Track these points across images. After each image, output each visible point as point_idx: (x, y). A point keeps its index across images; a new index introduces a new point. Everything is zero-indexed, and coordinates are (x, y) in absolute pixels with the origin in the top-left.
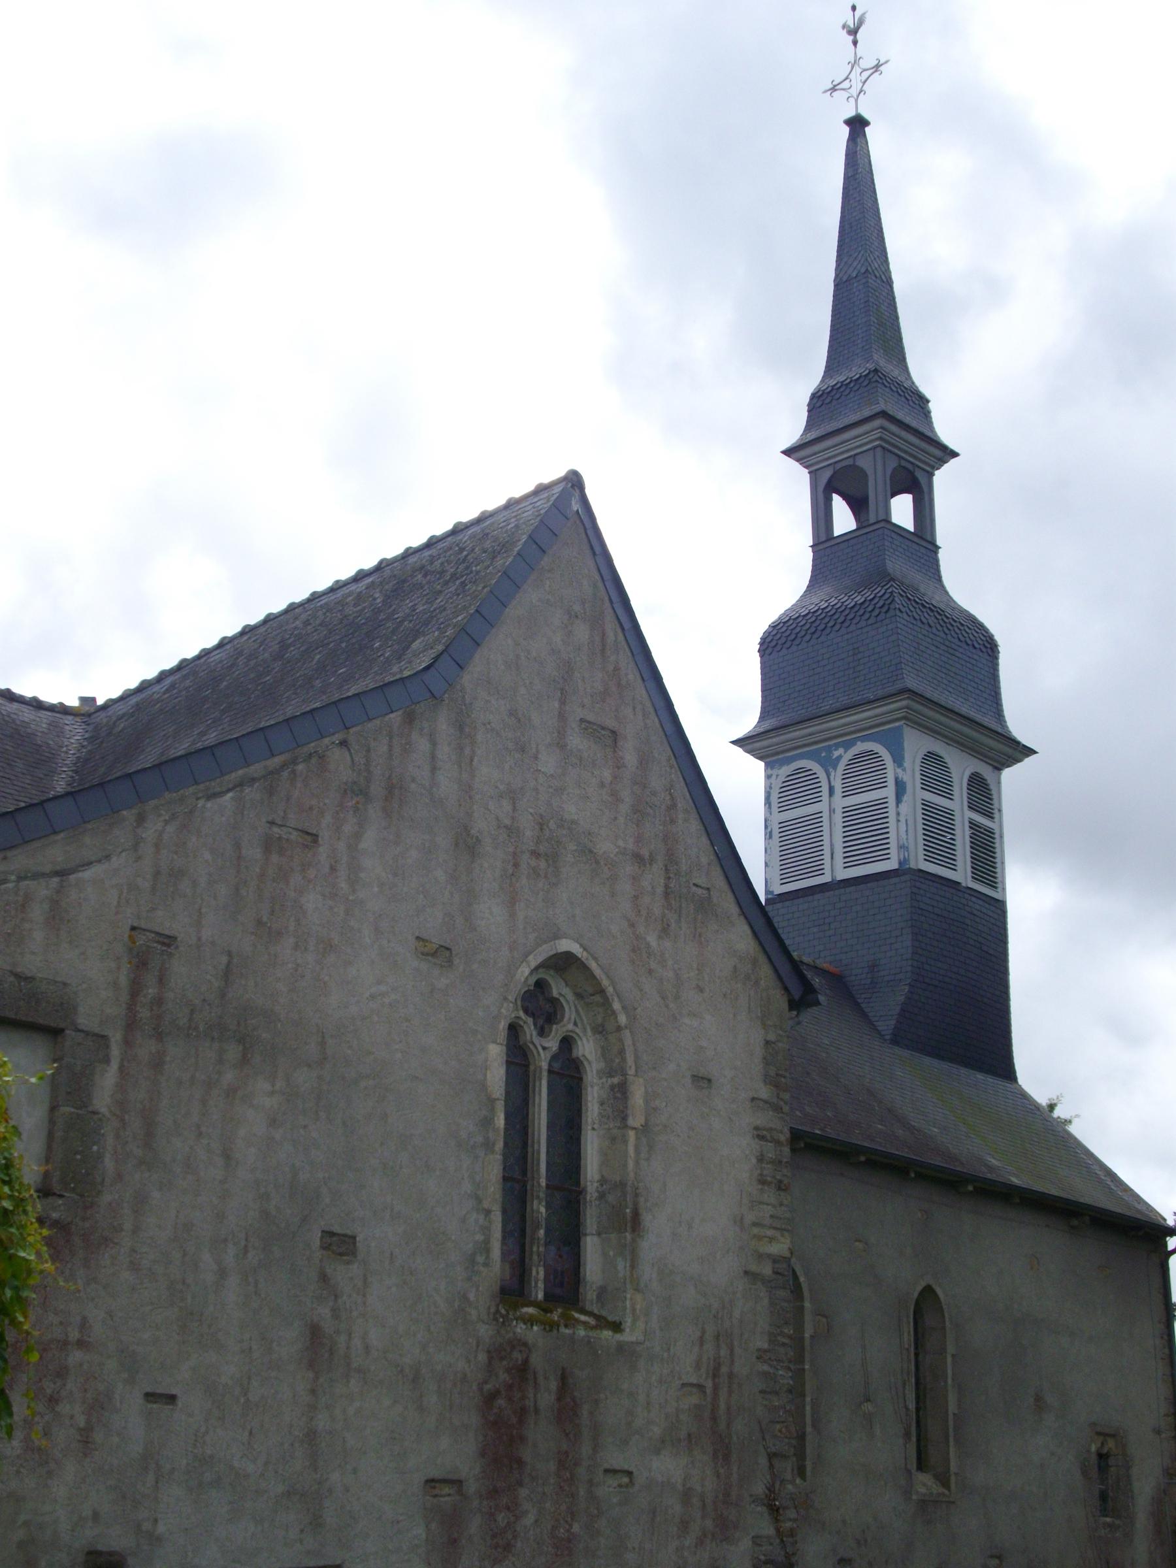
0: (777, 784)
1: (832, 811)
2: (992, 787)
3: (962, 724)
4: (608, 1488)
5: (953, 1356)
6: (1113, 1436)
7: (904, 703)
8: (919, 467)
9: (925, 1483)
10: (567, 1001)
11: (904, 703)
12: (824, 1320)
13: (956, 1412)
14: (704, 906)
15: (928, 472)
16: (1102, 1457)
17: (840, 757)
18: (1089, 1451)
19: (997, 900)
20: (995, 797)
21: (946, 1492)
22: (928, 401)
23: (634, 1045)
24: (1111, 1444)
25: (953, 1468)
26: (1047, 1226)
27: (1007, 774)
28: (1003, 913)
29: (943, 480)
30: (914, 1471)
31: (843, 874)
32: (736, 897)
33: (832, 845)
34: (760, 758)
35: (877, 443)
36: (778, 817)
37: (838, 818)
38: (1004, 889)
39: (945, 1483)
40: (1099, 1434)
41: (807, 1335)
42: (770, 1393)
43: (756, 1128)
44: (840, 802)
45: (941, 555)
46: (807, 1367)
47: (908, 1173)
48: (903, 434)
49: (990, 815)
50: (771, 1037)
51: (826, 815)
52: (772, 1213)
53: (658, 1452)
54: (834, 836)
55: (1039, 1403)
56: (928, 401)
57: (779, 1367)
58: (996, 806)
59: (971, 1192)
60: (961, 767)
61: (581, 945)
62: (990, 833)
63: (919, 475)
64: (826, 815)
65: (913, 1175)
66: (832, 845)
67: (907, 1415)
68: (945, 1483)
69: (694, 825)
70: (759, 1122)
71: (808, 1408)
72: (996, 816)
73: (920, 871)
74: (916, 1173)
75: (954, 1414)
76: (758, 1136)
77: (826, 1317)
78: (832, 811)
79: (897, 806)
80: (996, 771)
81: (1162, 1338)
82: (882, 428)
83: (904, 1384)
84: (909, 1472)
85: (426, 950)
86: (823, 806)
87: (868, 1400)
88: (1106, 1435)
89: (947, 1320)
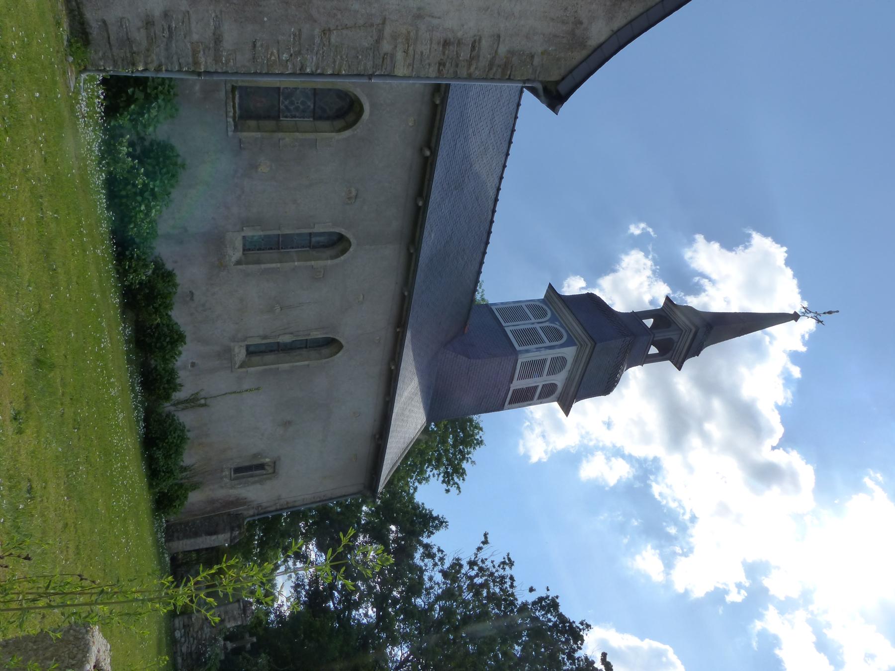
0: (538, 303)
1: (533, 324)
3: (580, 375)
5: (308, 365)
6: (274, 472)
8: (674, 352)
9: (240, 354)
12: (321, 276)
13: (280, 370)
15: (671, 358)
16: (261, 467)
17: (557, 325)
18: (266, 457)
20: (547, 399)
21: (237, 366)
22: (698, 356)
24: (270, 470)
26: (375, 421)
27: (555, 405)
28: (499, 410)
30: (246, 343)
31: (508, 330)
32: (623, 27)
34: (545, 296)
35: (683, 329)
36: (523, 305)
39: (241, 366)
40: (275, 463)
42: (300, 44)
44: (538, 326)
46: (296, 263)
47: (398, 327)
48: (689, 341)
49: (539, 398)
51: (530, 321)
52: (424, 51)
54: (523, 325)
55: (287, 424)
56: (698, 356)
58: (544, 400)
59: (391, 368)
60: (559, 379)
62: (532, 399)
63: (669, 355)
64: (530, 321)
65: (398, 330)
67: (275, 336)
68: (241, 366)
71: (274, 265)
72: (540, 401)
73: (518, 360)
74: (399, 332)
75: (278, 369)
76: (475, 41)
77: (323, 277)
78: (533, 324)
80: (557, 399)
81: (324, 496)
86: (533, 320)
87: (281, 309)
88: (274, 467)
89: (327, 360)
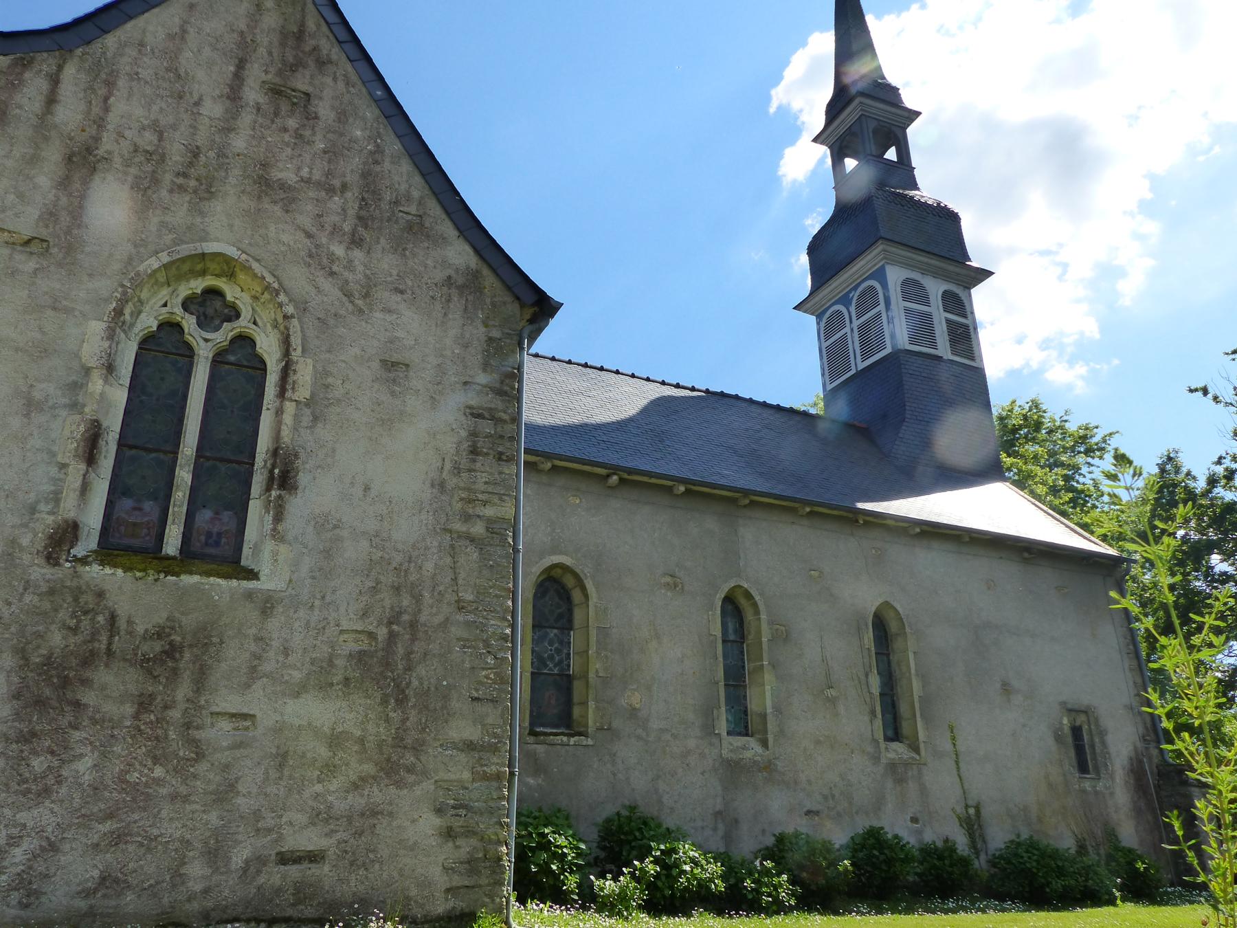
2: (965, 301)
4: (219, 733)
6: (1085, 712)
7: (881, 248)
9: (898, 750)
10: (244, 304)
11: (881, 248)
13: (922, 695)
14: (417, 228)
16: (1076, 731)
19: (977, 368)
21: (918, 758)
23: (302, 332)
25: (922, 735)
29: (913, 132)
31: (861, 366)
33: (854, 351)
37: (856, 330)
38: (982, 361)
40: (1070, 711)
41: (764, 640)
43: (470, 407)
45: (916, 172)
50: (496, 334)
51: (849, 334)
53: (297, 695)
54: (854, 344)
57: (490, 617)
60: (935, 288)
61: (239, 249)
64: (849, 334)
65: (862, 522)
66: (854, 351)
69: (406, 166)
70: (472, 403)
77: (784, 626)
79: (887, 312)
80: (967, 290)
82: (861, 103)
83: (867, 676)
84: (876, 741)
85: (12, 240)
86: (847, 329)
